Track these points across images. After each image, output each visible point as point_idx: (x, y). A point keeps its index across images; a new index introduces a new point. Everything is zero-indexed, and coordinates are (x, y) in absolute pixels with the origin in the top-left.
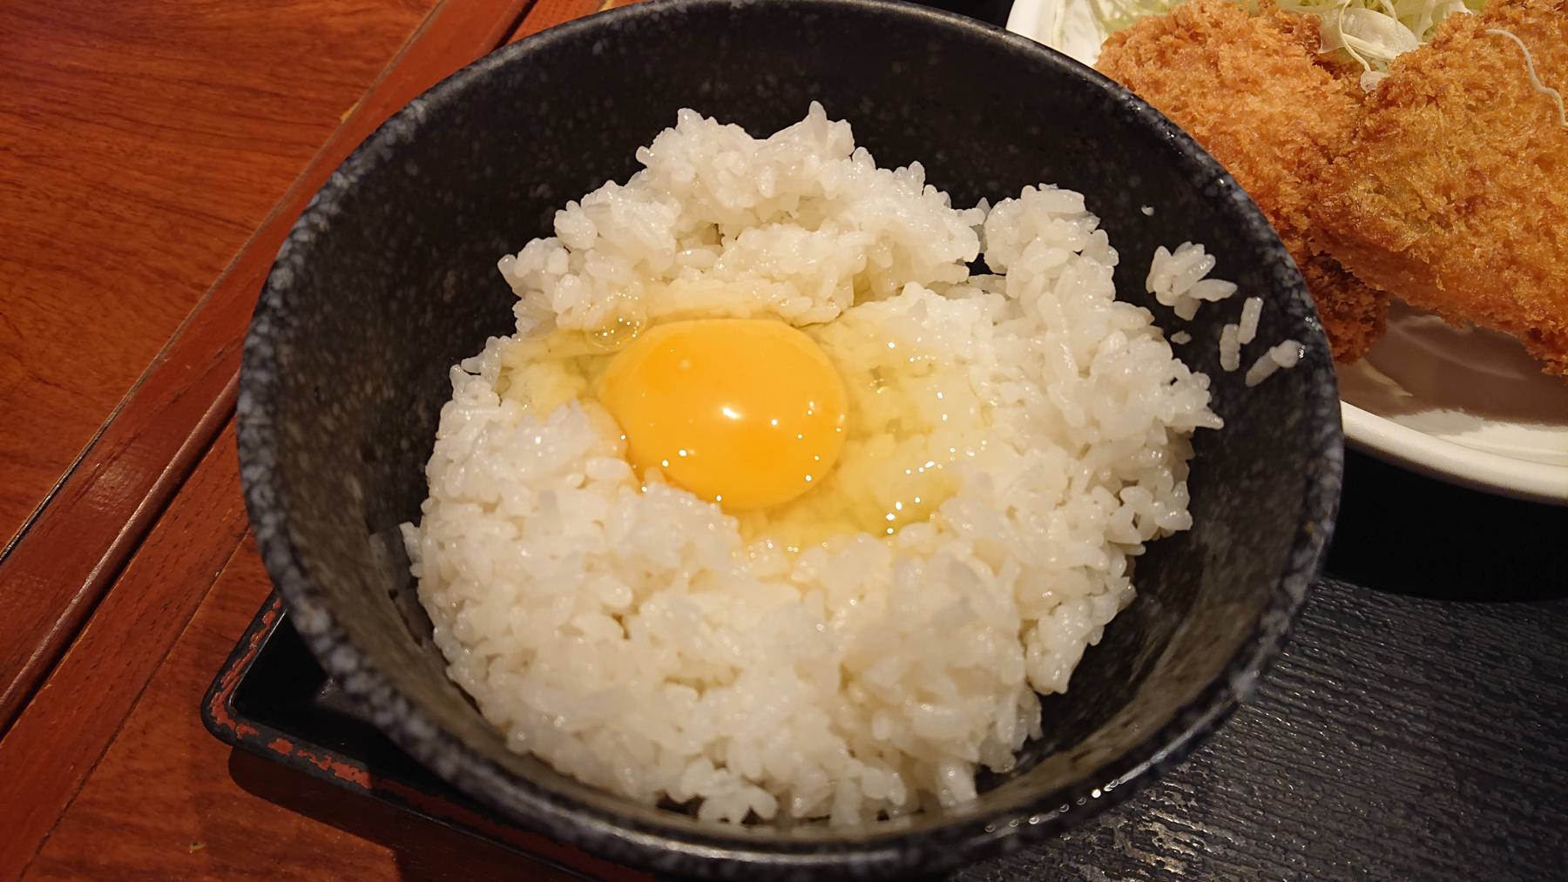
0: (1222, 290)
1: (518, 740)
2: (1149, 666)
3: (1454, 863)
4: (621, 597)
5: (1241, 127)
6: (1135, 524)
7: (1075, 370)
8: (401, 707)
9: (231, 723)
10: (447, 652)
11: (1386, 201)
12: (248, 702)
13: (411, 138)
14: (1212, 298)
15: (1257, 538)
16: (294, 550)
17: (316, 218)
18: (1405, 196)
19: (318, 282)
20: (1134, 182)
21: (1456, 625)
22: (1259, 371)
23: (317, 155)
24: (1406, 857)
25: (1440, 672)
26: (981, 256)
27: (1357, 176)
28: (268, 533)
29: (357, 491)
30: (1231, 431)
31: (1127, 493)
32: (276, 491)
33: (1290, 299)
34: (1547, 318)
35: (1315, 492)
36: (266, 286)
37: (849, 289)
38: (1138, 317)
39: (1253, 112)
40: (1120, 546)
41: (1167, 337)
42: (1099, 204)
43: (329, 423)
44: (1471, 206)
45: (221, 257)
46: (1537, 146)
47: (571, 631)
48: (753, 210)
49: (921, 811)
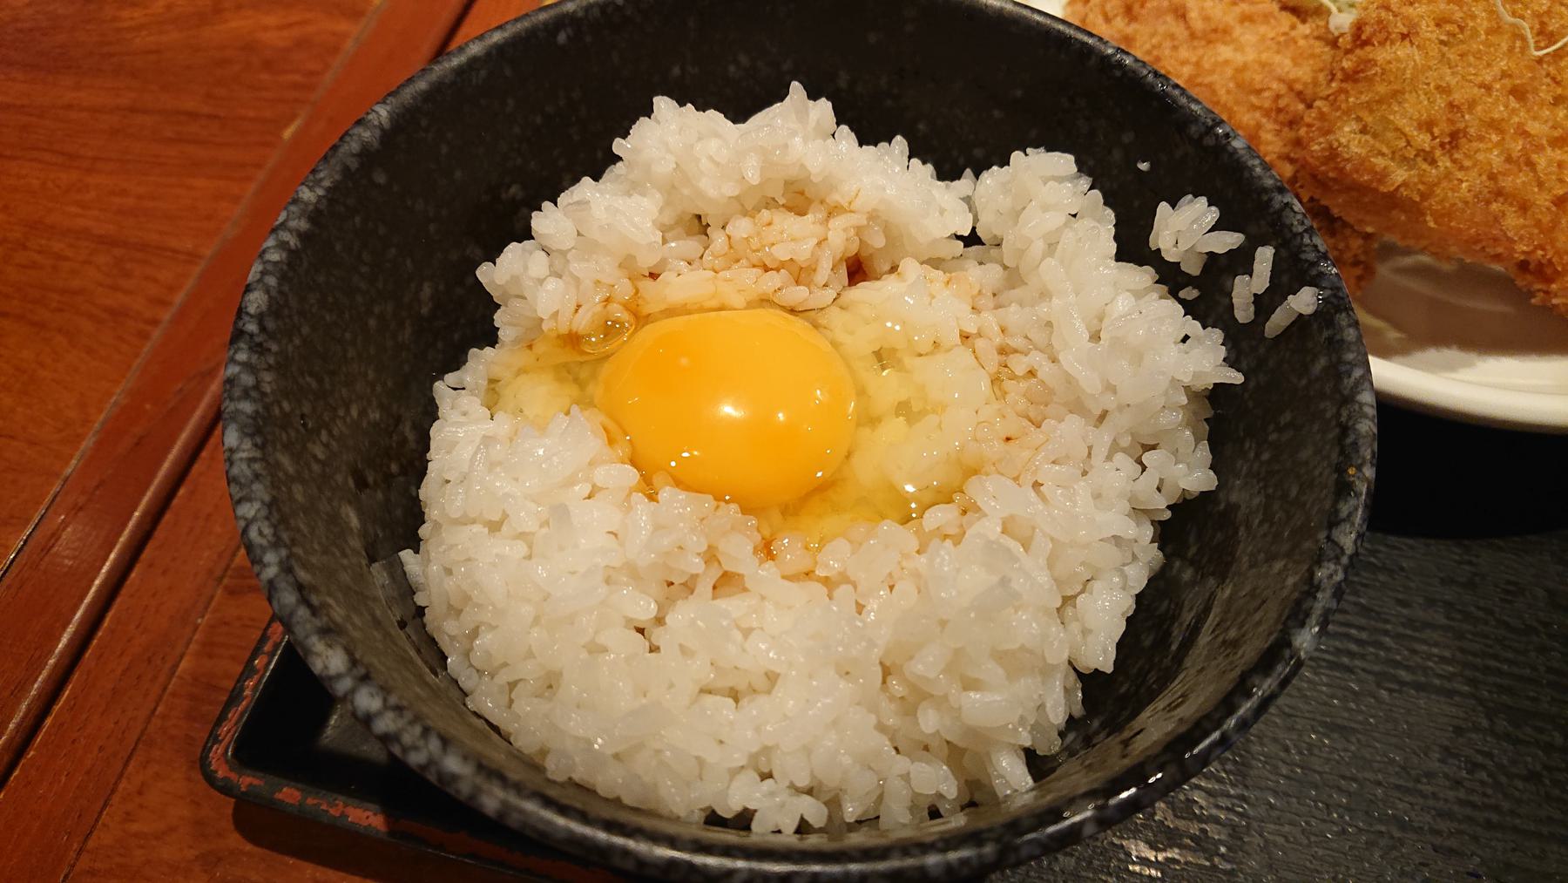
0: (1229, 241)
1: (555, 769)
2: (1194, 631)
3: (1493, 801)
4: (645, 610)
5: (1215, 77)
6: (1159, 489)
7: (1086, 336)
8: (434, 745)
9: (233, 776)
10: (465, 683)
11: (1372, 141)
12: (248, 752)
13: (376, 144)
14: (1221, 250)
15: (1294, 492)
16: (300, 587)
17: (285, 236)
18: (1390, 135)
19: (293, 302)
20: (1127, 138)
21: (1470, 563)
22: (1278, 320)
23: (261, 175)
24: (1446, 800)
25: (1460, 611)
26: (974, 229)
28: (271, 572)
29: (354, 521)
30: (1252, 384)
31: (1147, 458)
32: (275, 527)
33: (1302, 244)
34: (1536, 248)
35: (1349, 440)
36: (241, 312)
37: (843, 272)
38: (1143, 276)
39: (1226, 62)
40: (1145, 511)
41: (1174, 293)
42: (1091, 163)
43: (319, 452)
44: (1454, 140)
45: (172, 289)
46: (1510, 76)
47: (596, 649)
48: (737, 198)
49: (972, 804)
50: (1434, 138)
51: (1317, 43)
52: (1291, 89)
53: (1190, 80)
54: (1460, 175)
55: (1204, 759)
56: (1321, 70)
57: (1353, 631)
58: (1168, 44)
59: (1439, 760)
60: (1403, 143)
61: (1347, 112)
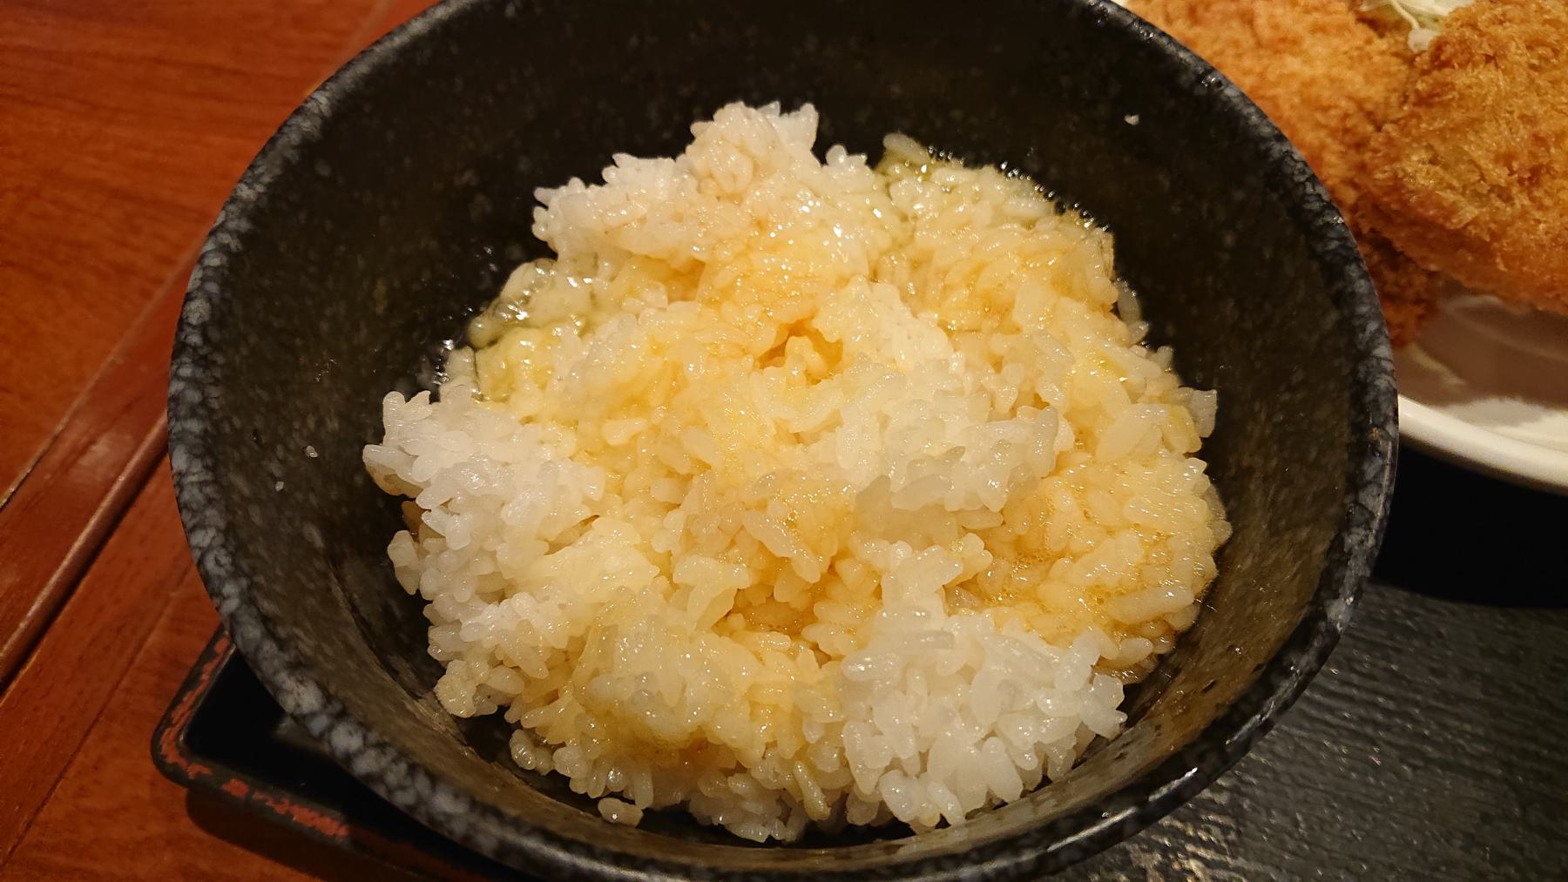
5: (1280, 91)
8: (422, 783)
13: (316, 133)
16: (266, 620)
17: (225, 238)
27: (1409, 145)
28: (232, 604)
32: (232, 555)
36: (182, 323)
39: (1293, 75)
44: (1534, 177)
50: (1512, 173)
51: (1394, 60)
52: (1360, 107)
53: (1253, 89)
54: (1538, 215)
55: (1246, 746)
56: (1395, 90)
57: (1380, 700)
58: (1230, 52)
59: (1461, 848)
60: (1476, 177)
61: (1417, 140)
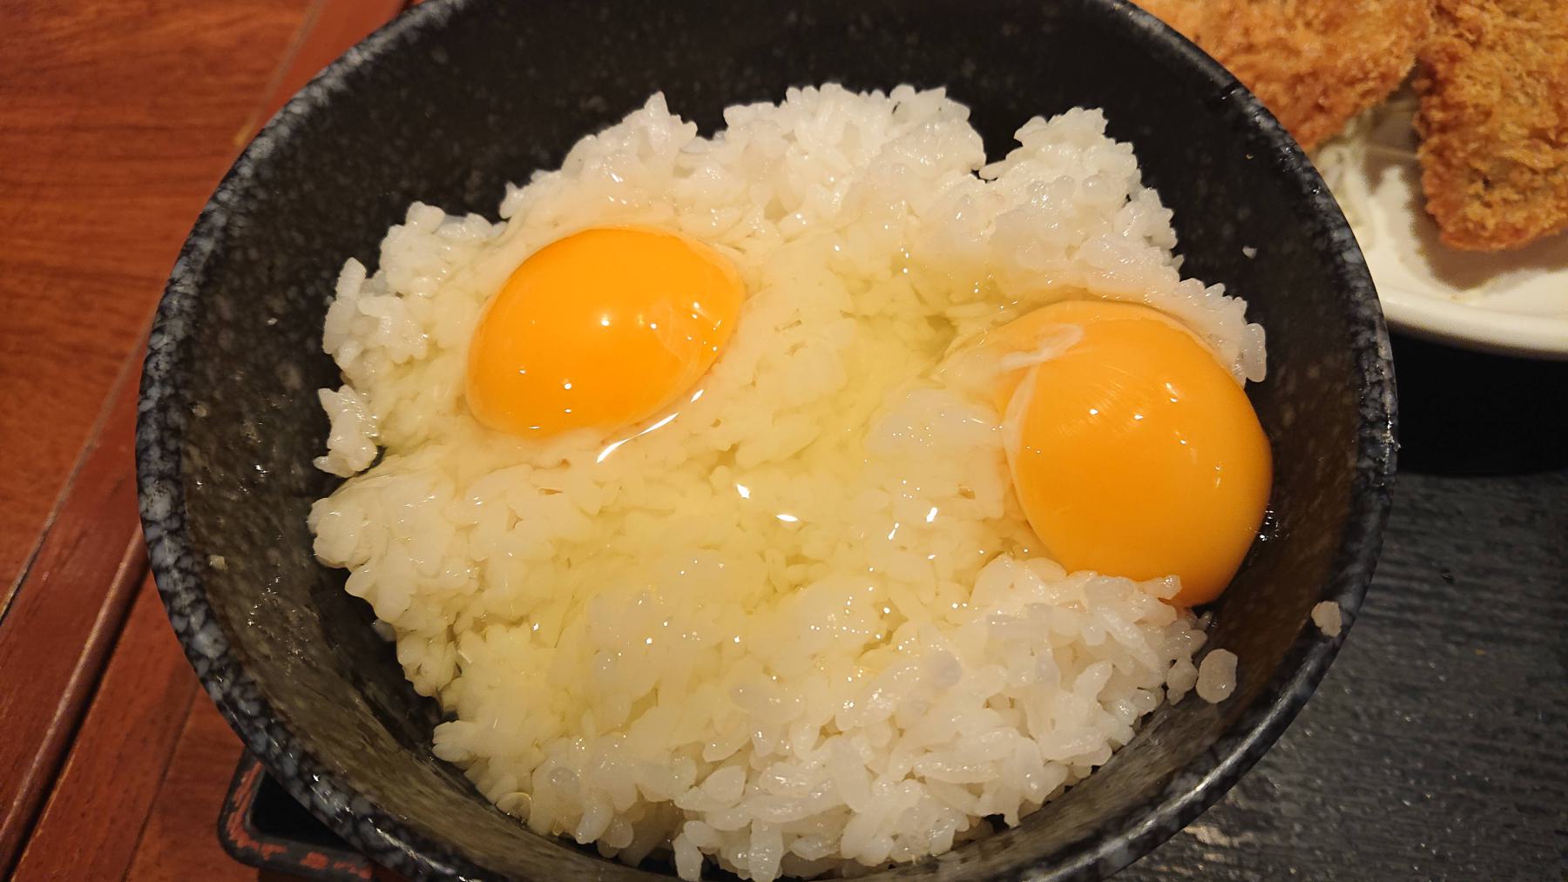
9: (254, 845)
19: (302, 157)
